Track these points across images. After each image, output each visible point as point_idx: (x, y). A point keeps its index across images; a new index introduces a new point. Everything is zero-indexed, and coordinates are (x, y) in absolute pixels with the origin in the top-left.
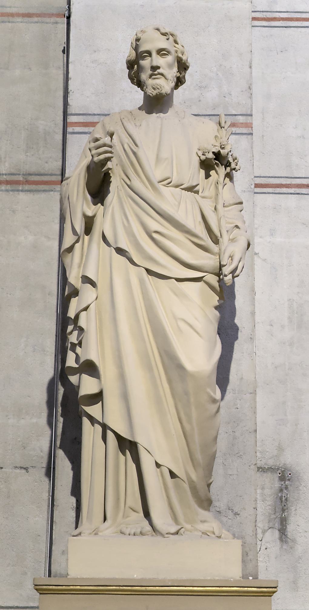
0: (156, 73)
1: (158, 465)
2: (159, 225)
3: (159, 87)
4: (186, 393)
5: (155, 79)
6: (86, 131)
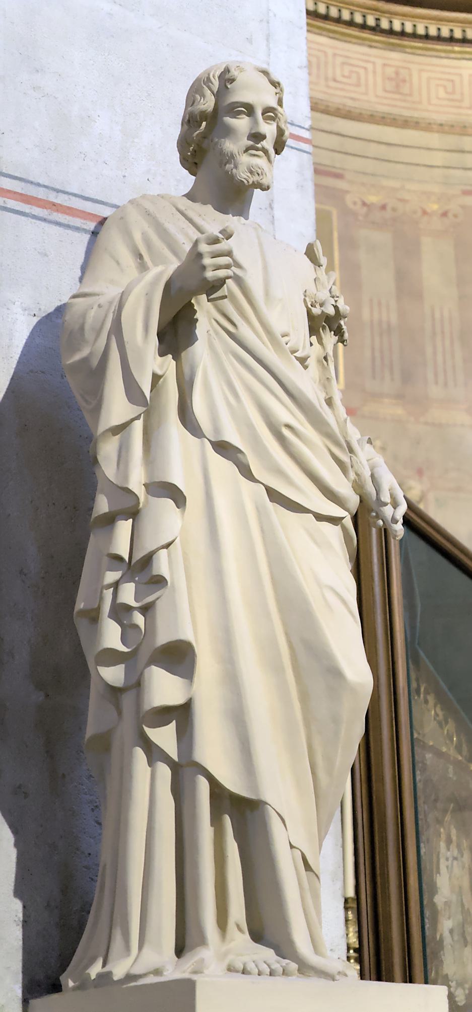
0: (259, 146)
1: (292, 847)
2: (288, 413)
3: (260, 172)
4: (336, 720)
5: (254, 155)
6: (27, 211)
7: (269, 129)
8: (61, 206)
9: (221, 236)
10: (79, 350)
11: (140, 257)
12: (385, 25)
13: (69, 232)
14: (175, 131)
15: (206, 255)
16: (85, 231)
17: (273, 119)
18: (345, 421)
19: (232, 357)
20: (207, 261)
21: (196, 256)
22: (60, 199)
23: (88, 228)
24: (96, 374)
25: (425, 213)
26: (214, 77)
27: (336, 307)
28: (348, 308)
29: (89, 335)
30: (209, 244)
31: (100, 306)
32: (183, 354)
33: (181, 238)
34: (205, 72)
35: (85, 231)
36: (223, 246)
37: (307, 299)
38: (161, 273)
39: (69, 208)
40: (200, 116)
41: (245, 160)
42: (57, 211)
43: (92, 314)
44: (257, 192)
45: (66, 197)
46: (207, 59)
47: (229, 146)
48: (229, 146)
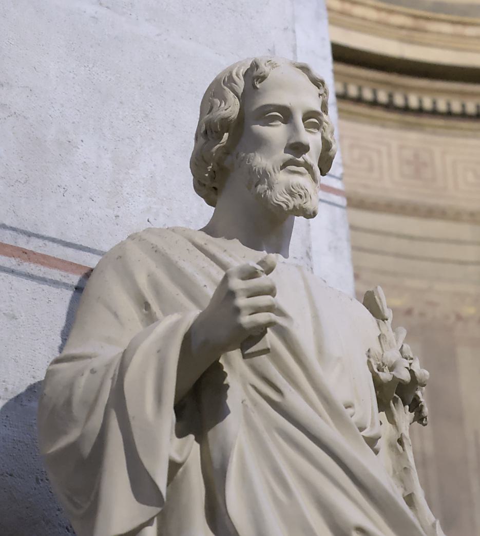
0: (301, 159)
3: (302, 193)
7: (313, 139)
8: (34, 253)
9: (259, 268)
10: (66, 433)
11: (147, 306)
12: (399, 100)
13: (45, 287)
14: (189, 145)
15: (240, 293)
16: (66, 285)
17: (317, 126)
18: (434, 525)
19: (276, 435)
20: (241, 301)
21: (226, 295)
22: (33, 245)
23: (70, 282)
24: (87, 466)
25: (459, 318)
26: (237, 75)
27: (411, 372)
28: (427, 373)
29: (78, 411)
30: (243, 279)
31: (93, 371)
32: (210, 434)
33: (201, 280)
34: (224, 72)
35: (66, 285)
36: (263, 280)
37: (371, 360)
38: (177, 324)
39: (44, 256)
40: (221, 126)
41: (282, 178)
42: (29, 260)
43: (82, 382)
44: (299, 221)
45: (40, 242)
46: (230, 57)
47: (260, 161)
48: (260, 161)
